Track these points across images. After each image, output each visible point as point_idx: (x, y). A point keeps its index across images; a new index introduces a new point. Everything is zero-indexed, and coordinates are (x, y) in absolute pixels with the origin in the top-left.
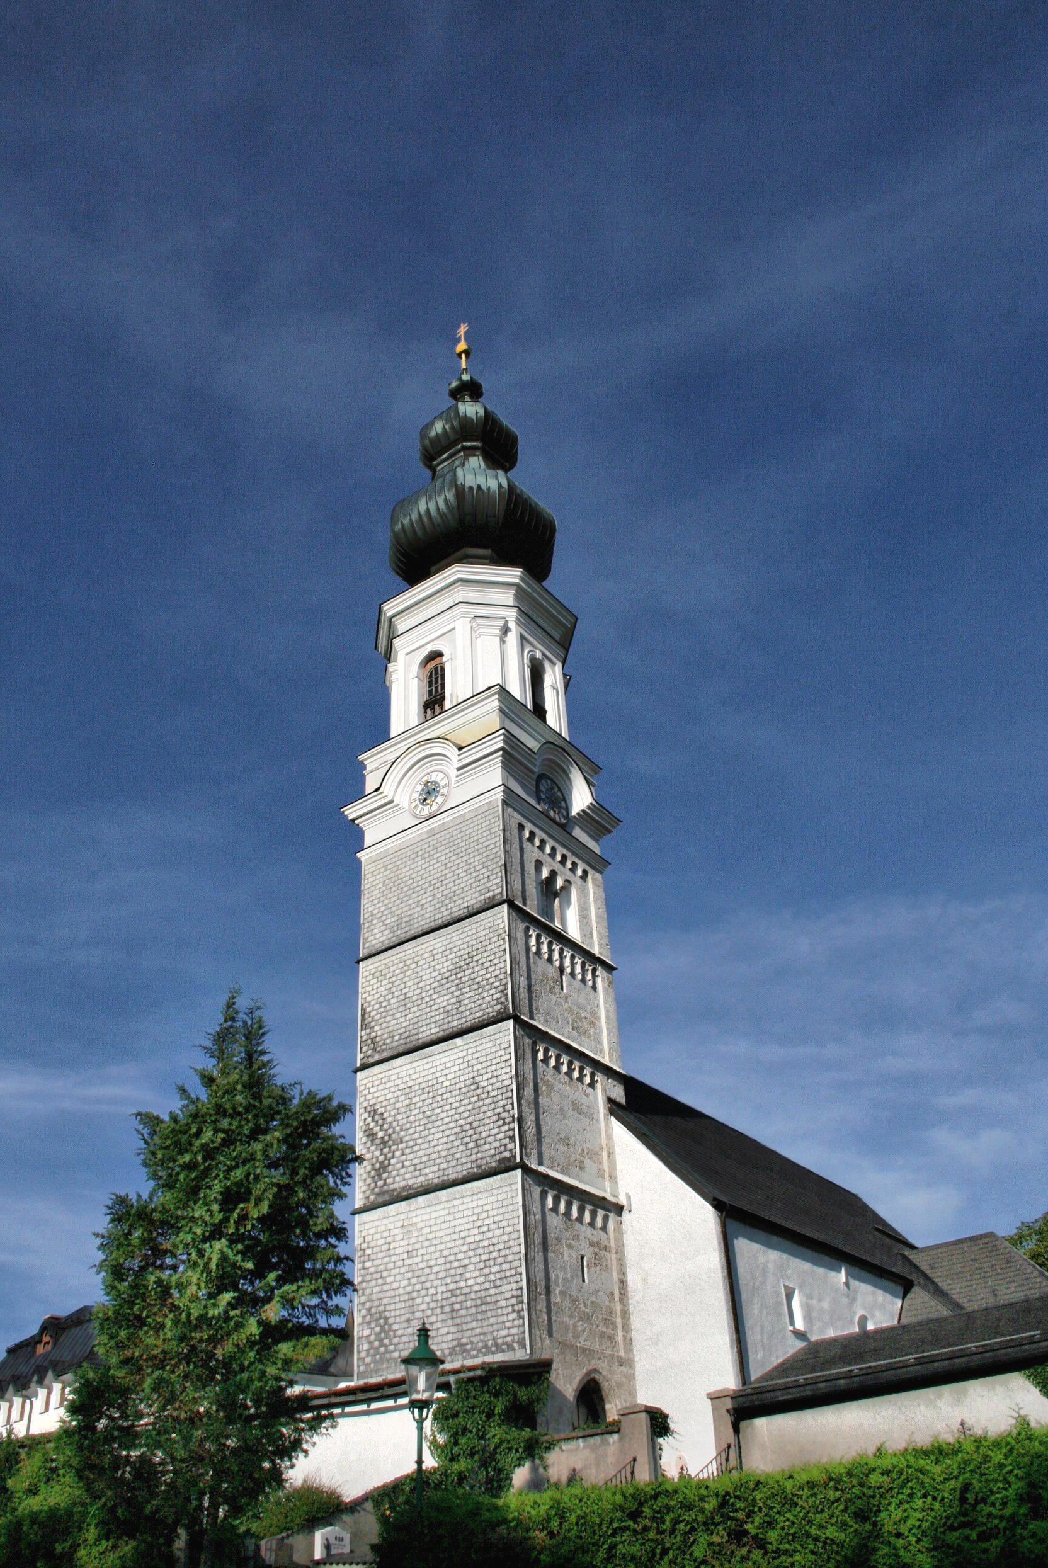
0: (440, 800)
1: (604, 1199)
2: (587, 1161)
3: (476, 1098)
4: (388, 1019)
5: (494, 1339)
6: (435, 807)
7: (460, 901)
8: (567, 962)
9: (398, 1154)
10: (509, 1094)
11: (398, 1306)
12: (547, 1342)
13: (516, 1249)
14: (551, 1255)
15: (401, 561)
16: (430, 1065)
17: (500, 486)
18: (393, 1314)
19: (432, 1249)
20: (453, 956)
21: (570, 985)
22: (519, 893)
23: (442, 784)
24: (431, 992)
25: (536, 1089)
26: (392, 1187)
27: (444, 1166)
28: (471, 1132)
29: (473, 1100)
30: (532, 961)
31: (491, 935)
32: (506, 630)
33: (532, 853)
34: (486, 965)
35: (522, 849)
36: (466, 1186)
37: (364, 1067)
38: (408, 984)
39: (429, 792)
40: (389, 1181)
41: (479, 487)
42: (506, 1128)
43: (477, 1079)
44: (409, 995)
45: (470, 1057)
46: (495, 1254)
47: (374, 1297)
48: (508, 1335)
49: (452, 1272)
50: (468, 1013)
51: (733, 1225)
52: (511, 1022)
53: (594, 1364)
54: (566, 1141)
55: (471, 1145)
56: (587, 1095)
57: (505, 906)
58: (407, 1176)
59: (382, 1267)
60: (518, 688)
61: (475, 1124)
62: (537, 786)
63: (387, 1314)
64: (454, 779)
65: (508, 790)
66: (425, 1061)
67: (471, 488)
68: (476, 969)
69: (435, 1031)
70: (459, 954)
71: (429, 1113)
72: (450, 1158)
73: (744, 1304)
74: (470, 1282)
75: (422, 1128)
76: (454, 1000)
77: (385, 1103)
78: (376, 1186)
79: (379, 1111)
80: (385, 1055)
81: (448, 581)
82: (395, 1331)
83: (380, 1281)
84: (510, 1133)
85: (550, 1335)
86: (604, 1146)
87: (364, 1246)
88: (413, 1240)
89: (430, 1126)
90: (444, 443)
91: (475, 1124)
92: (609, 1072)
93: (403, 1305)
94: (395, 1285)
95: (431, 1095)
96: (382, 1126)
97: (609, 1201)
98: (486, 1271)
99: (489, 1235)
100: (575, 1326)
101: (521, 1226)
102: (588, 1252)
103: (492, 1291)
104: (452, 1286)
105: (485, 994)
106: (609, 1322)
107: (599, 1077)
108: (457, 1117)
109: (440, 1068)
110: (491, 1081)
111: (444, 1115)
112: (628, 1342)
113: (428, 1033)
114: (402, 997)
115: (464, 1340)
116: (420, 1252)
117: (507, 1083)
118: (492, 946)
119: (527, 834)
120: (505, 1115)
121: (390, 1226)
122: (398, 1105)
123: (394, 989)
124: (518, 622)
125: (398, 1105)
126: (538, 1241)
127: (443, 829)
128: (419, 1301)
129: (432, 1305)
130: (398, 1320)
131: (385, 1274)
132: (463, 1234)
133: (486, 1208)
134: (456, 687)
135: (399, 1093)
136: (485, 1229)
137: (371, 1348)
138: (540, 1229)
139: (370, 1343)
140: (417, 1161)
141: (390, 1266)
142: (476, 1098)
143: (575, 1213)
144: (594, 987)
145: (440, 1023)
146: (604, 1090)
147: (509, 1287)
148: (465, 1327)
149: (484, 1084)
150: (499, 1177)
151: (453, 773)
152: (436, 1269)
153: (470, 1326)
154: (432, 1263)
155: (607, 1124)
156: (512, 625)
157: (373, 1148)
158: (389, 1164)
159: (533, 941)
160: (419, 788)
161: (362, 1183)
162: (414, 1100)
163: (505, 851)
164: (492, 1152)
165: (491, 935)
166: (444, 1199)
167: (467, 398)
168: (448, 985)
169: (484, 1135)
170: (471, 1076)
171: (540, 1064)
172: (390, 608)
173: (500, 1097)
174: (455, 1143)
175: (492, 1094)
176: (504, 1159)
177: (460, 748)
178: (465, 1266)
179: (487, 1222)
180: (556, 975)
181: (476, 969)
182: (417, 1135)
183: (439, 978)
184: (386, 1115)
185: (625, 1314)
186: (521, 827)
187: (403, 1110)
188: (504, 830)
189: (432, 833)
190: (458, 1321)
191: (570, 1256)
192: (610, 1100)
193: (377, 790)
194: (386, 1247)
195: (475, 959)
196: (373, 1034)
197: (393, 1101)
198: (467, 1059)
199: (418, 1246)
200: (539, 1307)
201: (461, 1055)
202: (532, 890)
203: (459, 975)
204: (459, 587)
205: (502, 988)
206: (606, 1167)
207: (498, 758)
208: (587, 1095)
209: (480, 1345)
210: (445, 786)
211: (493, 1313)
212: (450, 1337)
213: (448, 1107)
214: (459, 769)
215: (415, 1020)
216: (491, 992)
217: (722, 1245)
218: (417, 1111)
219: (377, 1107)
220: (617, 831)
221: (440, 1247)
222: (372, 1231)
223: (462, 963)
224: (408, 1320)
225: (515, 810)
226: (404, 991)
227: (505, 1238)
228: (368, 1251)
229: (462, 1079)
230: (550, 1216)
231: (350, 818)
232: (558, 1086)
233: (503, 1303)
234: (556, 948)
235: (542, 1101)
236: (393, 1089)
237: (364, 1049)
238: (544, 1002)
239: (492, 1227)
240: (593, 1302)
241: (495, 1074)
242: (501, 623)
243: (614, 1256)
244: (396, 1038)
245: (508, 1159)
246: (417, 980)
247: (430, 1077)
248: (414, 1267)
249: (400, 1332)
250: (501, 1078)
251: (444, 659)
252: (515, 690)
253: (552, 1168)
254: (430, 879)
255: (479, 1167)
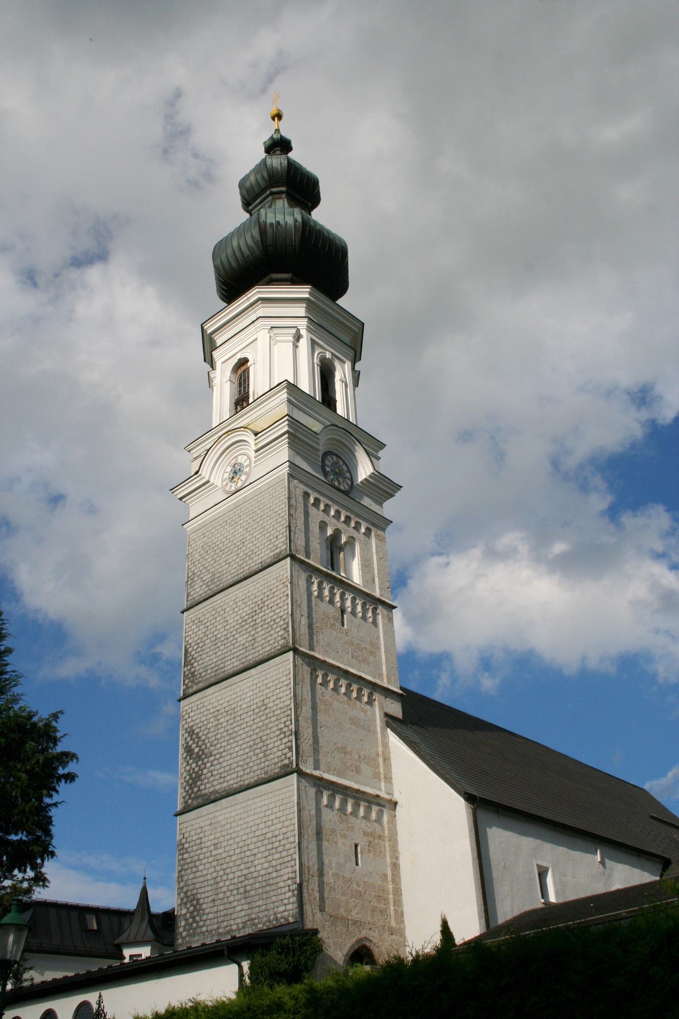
0: (243, 478)
1: (378, 796)
2: (363, 766)
3: (264, 717)
4: (203, 656)
5: (275, 914)
6: (240, 484)
7: (257, 558)
8: (348, 603)
9: (208, 765)
10: (289, 712)
11: (207, 889)
12: (319, 915)
13: (292, 839)
14: (325, 844)
15: (223, 289)
16: (232, 692)
17: (296, 221)
18: (203, 896)
19: (232, 841)
20: (250, 602)
21: (350, 622)
22: (302, 549)
23: (245, 465)
24: (234, 632)
25: (314, 707)
26: (204, 792)
27: (241, 773)
28: (261, 744)
29: (263, 718)
30: (313, 603)
31: (278, 583)
32: (298, 337)
33: (316, 515)
34: (274, 608)
35: (306, 514)
36: (257, 788)
37: (185, 697)
38: (219, 627)
39: (236, 472)
40: (202, 787)
41: (278, 223)
42: (286, 740)
43: (266, 701)
44: (219, 636)
45: (261, 684)
46: (276, 844)
47: (190, 882)
48: (285, 911)
49: (246, 860)
50: (260, 648)
51: (483, 815)
52: (291, 653)
53: (364, 933)
54: (344, 750)
55: (261, 755)
56: (365, 712)
57: (289, 559)
58: (215, 783)
59: (196, 858)
60: (307, 383)
61: (264, 738)
62: (323, 461)
63: (199, 896)
64: (253, 459)
65: (292, 465)
66: (229, 689)
67: (271, 224)
68: (267, 612)
69: (236, 665)
70: (255, 600)
71: (231, 731)
72: (245, 766)
73: (495, 881)
74: (258, 868)
75: (226, 743)
76: (250, 638)
77: (200, 725)
78: (192, 793)
79: (196, 731)
80: (201, 685)
81: (252, 301)
82: (204, 910)
83: (194, 869)
84: (289, 744)
85: (322, 910)
86: (380, 753)
87: (184, 841)
88: (218, 835)
89: (232, 741)
90: (257, 190)
91: (264, 738)
92: (387, 692)
93: (210, 888)
94: (205, 872)
95: (233, 716)
96: (197, 743)
97: (383, 798)
98: (270, 858)
99: (272, 828)
100: (347, 903)
101: (296, 821)
102: (362, 842)
103: (274, 875)
104: (245, 872)
105: (272, 632)
106: (381, 897)
107: (376, 696)
108: (251, 733)
109: (239, 694)
110: (276, 702)
111: (242, 732)
112: (400, 916)
113: (231, 666)
114: (214, 638)
115: (253, 916)
116: (223, 844)
117: (287, 703)
118: (278, 592)
119: (312, 500)
120: (285, 729)
121: (202, 824)
122: (209, 726)
123: (208, 633)
124: (309, 329)
125: (209, 726)
126: (312, 833)
127: (245, 501)
128: (221, 884)
129: (231, 887)
130: (206, 900)
131: (198, 863)
132: (254, 829)
133: (271, 806)
134: (258, 384)
135: (210, 716)
136: (269, 823)
137: (187, 924)
138: (314, 822)
139: (186, 920)
140: (222, 770)
141: (202, 856)
142: (264, 717)
143: (349, 809)
144: (375, 623)
145: (240, 657)
146: (381, 707)
147: (286, 871)
148: (254, 905)
149: (271, 705)
150: (282, 779)
151: (253, 454)
152: (234, 858)
153: (258, 904)
154: (231, 853)
155: (384, 735)
156: (303, 332)
157: (191, 761)
158: (202, 774)
159: (315, 587)
160: (229, 469)
161: (182, 790)
162: (221, 721)
163: (290, 515)
164: (276, 760)
165: (278, 583)
166: (240, 800)
167: (278, 152)
168: (247, 626)
169: (270, 746)
170: (262, 699)
171: (318, 687)
173: (282, 715)
174: (249, 754)
175: (276, 713)
176: (285, 765)
177: (256, 434)
178: (255, 855)
179: (271, 817)
180: (338, 614)
181: (267, 612)
182: (222, 749)
183: (240, 621)
184: (201, 734)
185: (398, 892)
186: (306, 495)
187: (212, 729)
188: (289, 498)
189: (237, 506)
190: (249, 900)
191: (344, 844)
192: (387, 715)
193: (196, 473)
194: (198, 842)
195: (266, 603)
196: (193, 670)
197: (205, 722)
198: (259, 685)
199: (222, 839)
200: (310, 887)
201: (255, 682)
202: (317, 546)
203: (254, 618)
204: (260, 305)
205: (285, 626)
206: (382, 770)
207: (285, 440)
208: (365, 712)
209: (265, 919)
210: (247, 466)
211: (275, 893)
212: (243, 913)
213: (244, 725)
214: (256, 451)
215: (223, 656)
216: (278, 630)
217: (473, 832)
218: (222, 730)
219: (194, 728)
221: (238, 840)
222: (189, 829)
223: (257, 608)
224: (214, 900)
225: (301, 481)
226: (216, 633)
227: (284, 830)
228: (186, 845)
229: (255, 702)
230: (326, 812)
232: (336, 704)
233: (281, 884)
234: (338, 592)
235: (321, 717)
236: (206, 713)
237: (186, 682)
238: (324, 637)
239: (275, 821)
240: (365, 882)
241: (279, 696)
242: (294, 331)
243: (387, 844)
244: (209, 672)
245: (287, 766)
246: (224, 624)
247: (232, 702)
248: (219, 857)
249: (207, 911)
250: (283, 699)
251: (249, 364)
252: (305, 385)
253: (328, 772)
254: (235, 542)
255: (266, 773)
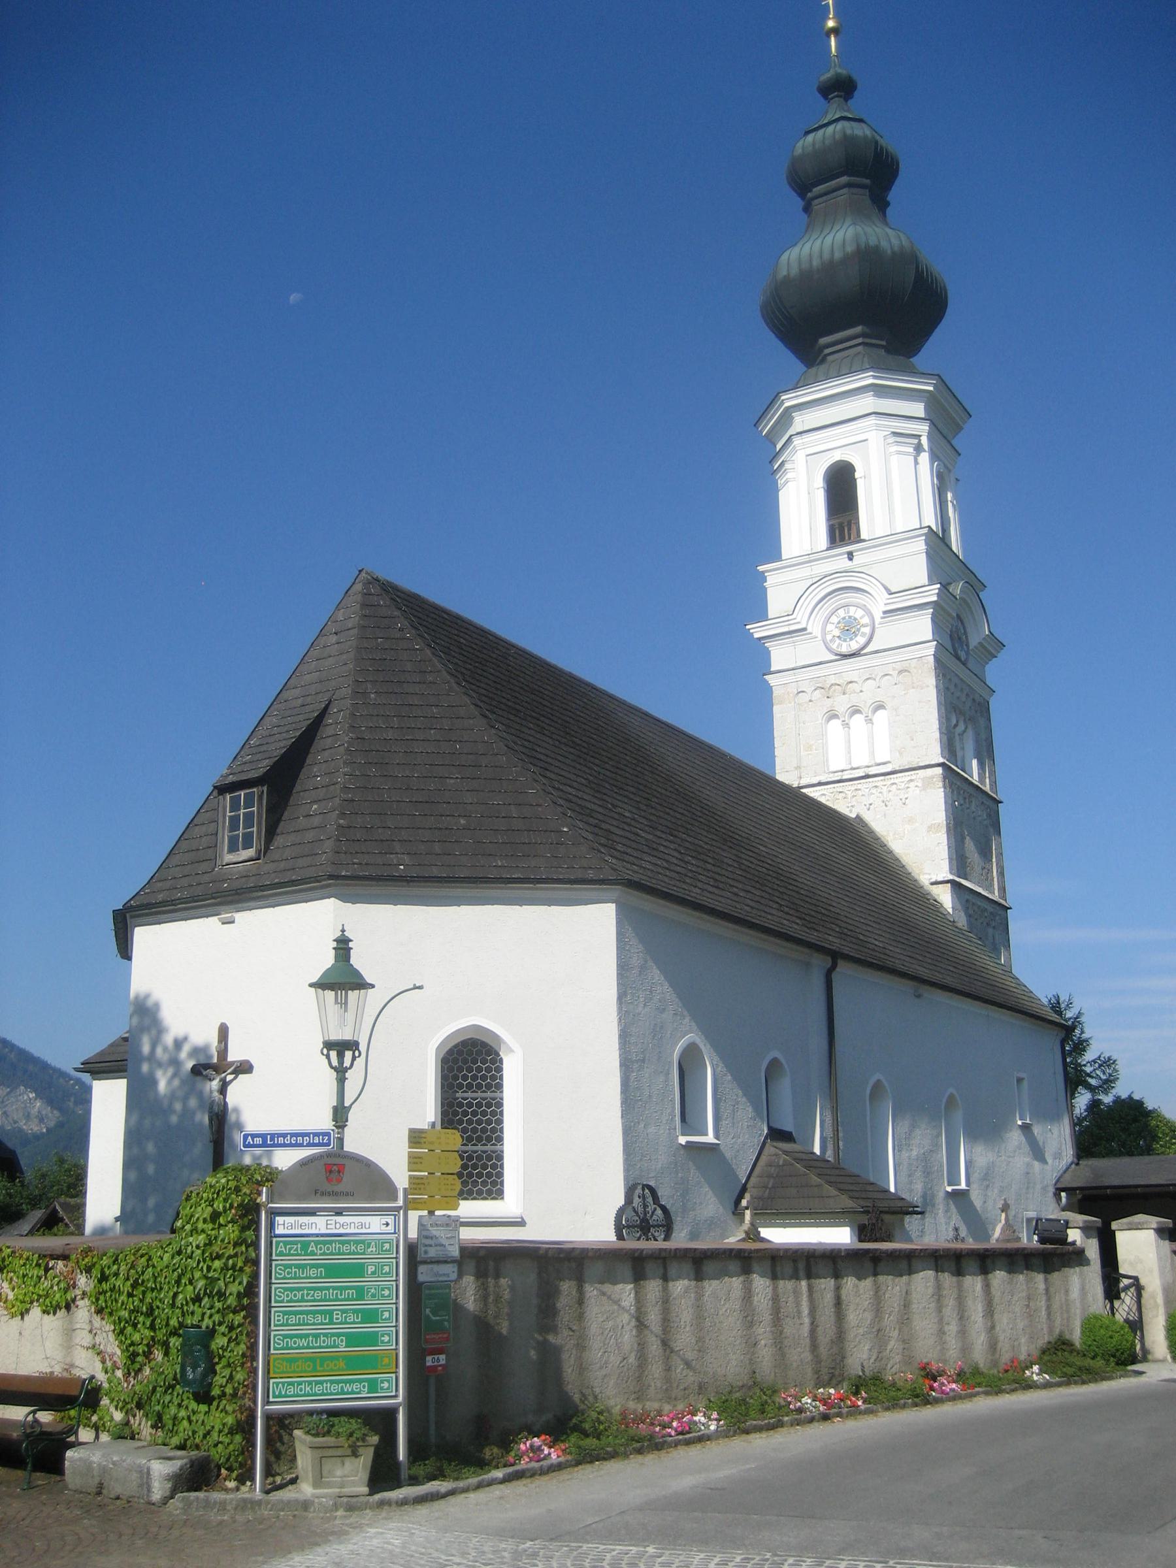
151: (878, 615)
172: (790, 399)
214: (885, 612)
220: (1003, 655)
231: (756, 636)
242: (916, 441)
252: (934, 528)
